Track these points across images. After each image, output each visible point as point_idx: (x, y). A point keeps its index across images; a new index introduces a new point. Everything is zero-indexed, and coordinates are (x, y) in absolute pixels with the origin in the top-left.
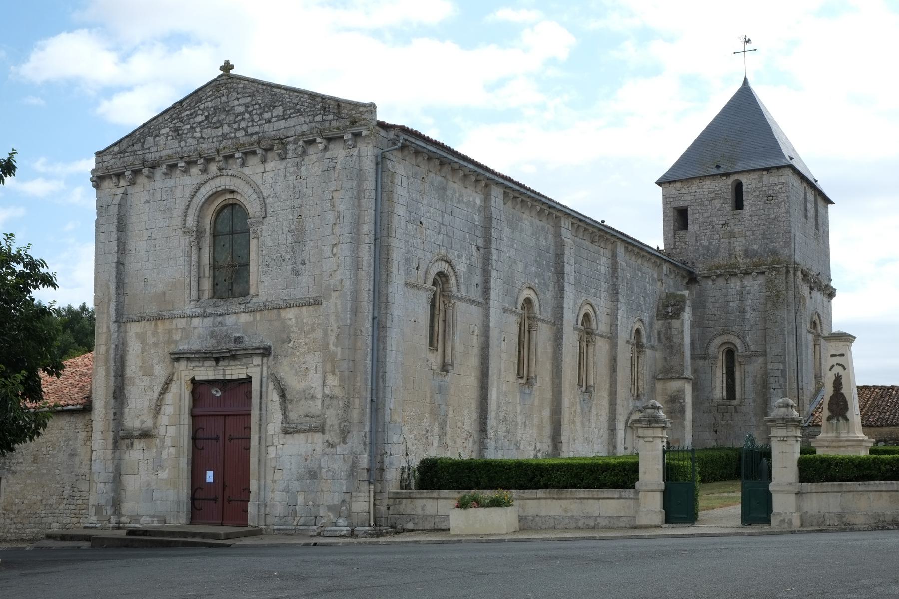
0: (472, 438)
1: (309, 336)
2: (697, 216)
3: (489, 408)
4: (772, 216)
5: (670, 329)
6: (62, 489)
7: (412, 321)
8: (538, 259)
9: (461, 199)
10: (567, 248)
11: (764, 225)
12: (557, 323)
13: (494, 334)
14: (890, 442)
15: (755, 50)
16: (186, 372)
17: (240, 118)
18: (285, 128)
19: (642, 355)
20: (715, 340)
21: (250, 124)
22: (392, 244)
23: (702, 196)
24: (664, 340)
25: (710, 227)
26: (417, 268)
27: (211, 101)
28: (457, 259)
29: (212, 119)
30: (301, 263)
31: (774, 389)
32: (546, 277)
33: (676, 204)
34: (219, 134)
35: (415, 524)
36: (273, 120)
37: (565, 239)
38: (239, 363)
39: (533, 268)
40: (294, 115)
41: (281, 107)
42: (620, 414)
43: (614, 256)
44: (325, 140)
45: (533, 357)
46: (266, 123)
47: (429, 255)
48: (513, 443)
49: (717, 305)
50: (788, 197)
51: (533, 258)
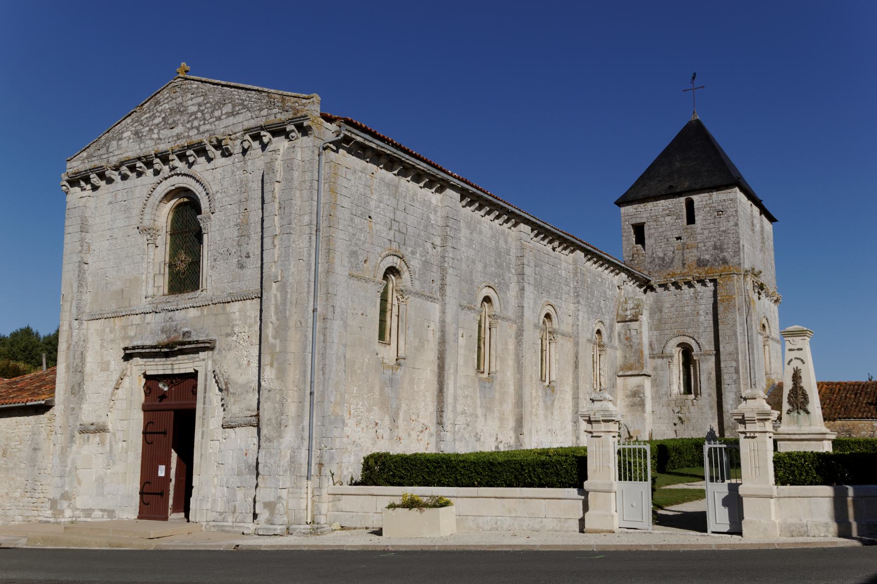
0: (428, 430)
1: (251, 329)
2: (652, 231)
3: (445, 401)
4: (722, 229)
5: (630, 330)
6: (25, 482)
7: (360, 314)
8: (498, 261)
9: (415, 197)
11: (715, 237)
12: (517, 321)
16: (139, 367)
17: (193, 117)
18: (233, 124)
19: (603, 353)
20: (672, 341)
21: (202, 123)
23: (657, 214)
25: (666, 240)
27: (167, 103)
28: (410, 255)
29: (168, 120)
30: (246, 257)
31: (729, 385)
32: (505, 278)
33: (634, 221)
34: (174, 134)
36: (224, 117)
39: (493, 269)
40: (242, 111)
41: (230, 104)
44: (268, 133)
45: (493, 352)
46: (216, 120)
47: (379, 250)
48: (473, 436)
49: (673, 309)
50: (736, 211)
51: (493, 259)
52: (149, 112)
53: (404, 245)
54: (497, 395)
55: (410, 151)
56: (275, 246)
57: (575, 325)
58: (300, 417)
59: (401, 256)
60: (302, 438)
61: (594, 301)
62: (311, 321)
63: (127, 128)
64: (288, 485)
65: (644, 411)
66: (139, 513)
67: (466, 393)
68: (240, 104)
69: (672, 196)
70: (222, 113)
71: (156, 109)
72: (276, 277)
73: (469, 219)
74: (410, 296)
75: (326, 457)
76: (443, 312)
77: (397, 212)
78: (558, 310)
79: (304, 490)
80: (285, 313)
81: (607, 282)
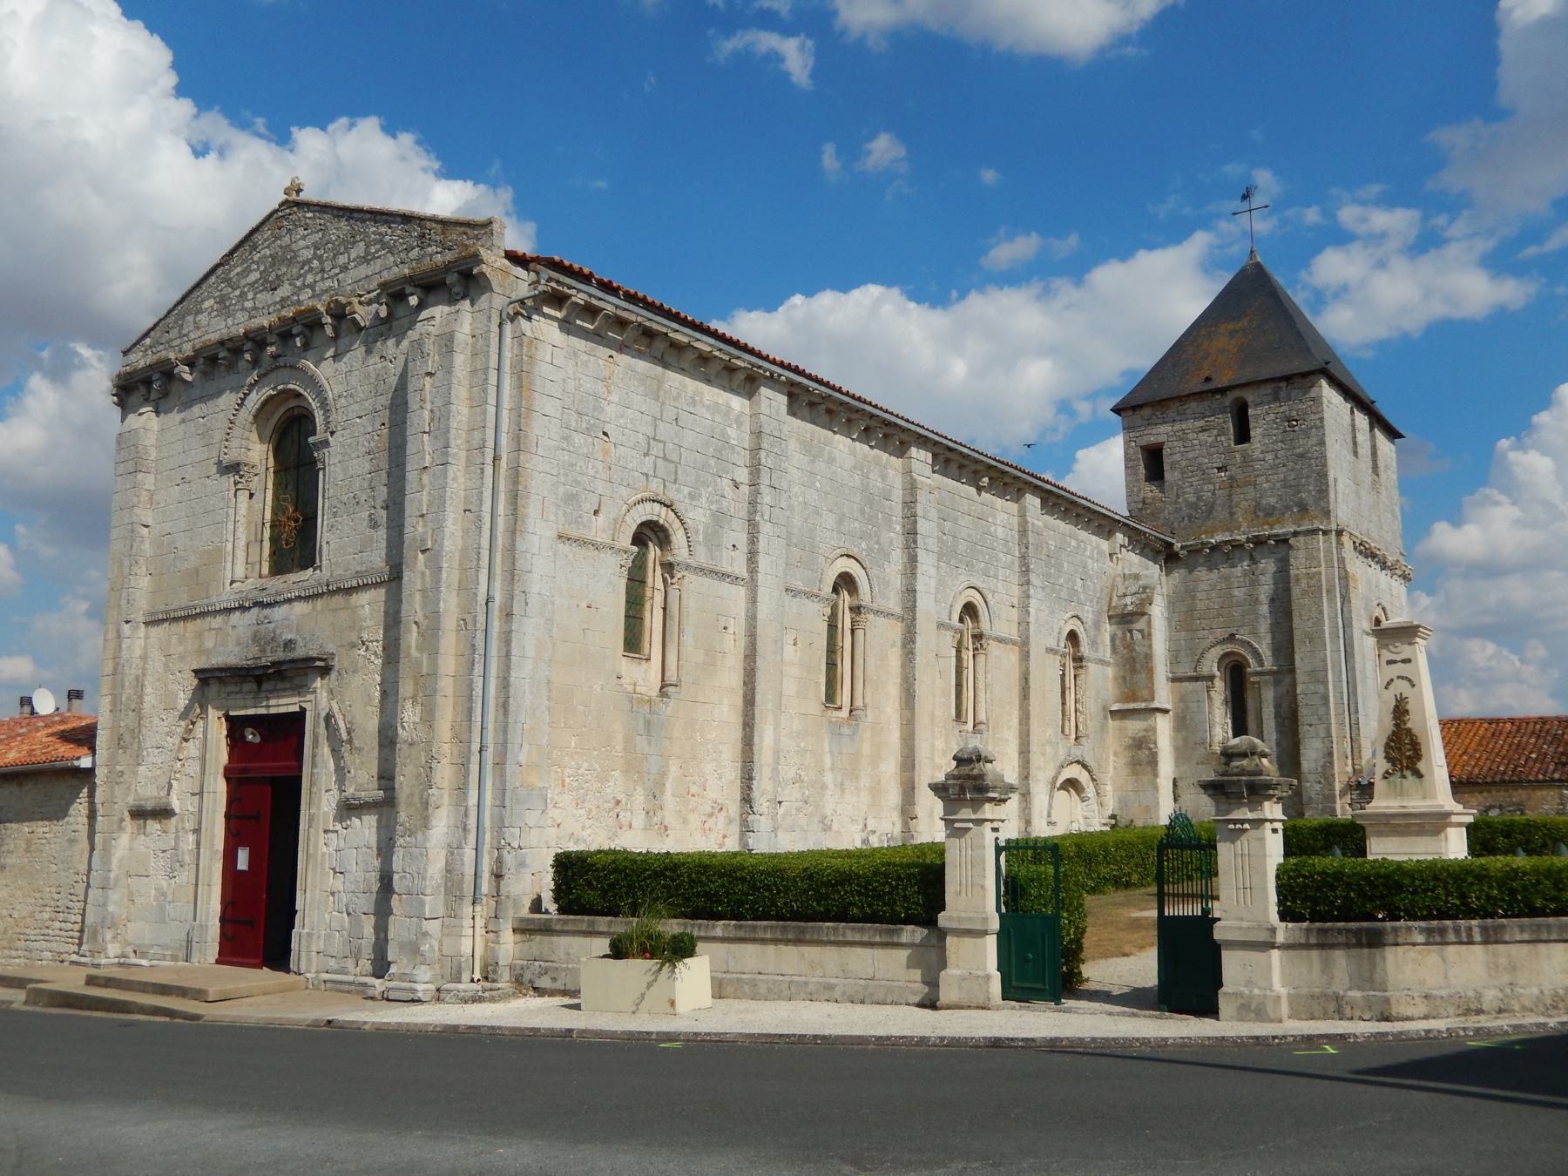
0: (724, 813)
7: (584, 605)
8: (867, 510)
9: (698, 399)
10: (922, 492)
13: (765, 633)
14: (1511, 809)
17: (306, 268)
19: (1081, 671)
21: (319, 277)
22: (527, 465)
24: (1120, 649)
26: (596, 512)
27: (268, 247)
35: (554, 979)
37: (918, 478)
38: (289, 686)
41: (363, 243)
42: (1039, 768)
43: (1022, 514)
44: (419, 290)
45: (859, 673)
46: (341, 272)
47: (624, 491)
48: (816, 821)
52: (242, 264)
53: (675, 482)
54: (866, 749)
55: (683, 315)
56: (423, 487)
57: (1024, 624)
58: (462, 790)
59: (667, 502)
60: (465, 829)
61: (1062, 581)
62: (481, 619)
63: (209, 292)
64: (441, 911)
65: (1156, 775)
66: (219, 953)
67: (802, 745)
68: (376, 242)
69: (1210, 394)
70: (349, 259)
71: (252, 259)
72: (423, 541)
73: (808, 435)
74: (686, 573)
75: (509, 859)
76: (753, 601)
77: (661, 425)
78: (989, 597)
79: (467, 922)
80: (438, 604)
81: (1089, 547)
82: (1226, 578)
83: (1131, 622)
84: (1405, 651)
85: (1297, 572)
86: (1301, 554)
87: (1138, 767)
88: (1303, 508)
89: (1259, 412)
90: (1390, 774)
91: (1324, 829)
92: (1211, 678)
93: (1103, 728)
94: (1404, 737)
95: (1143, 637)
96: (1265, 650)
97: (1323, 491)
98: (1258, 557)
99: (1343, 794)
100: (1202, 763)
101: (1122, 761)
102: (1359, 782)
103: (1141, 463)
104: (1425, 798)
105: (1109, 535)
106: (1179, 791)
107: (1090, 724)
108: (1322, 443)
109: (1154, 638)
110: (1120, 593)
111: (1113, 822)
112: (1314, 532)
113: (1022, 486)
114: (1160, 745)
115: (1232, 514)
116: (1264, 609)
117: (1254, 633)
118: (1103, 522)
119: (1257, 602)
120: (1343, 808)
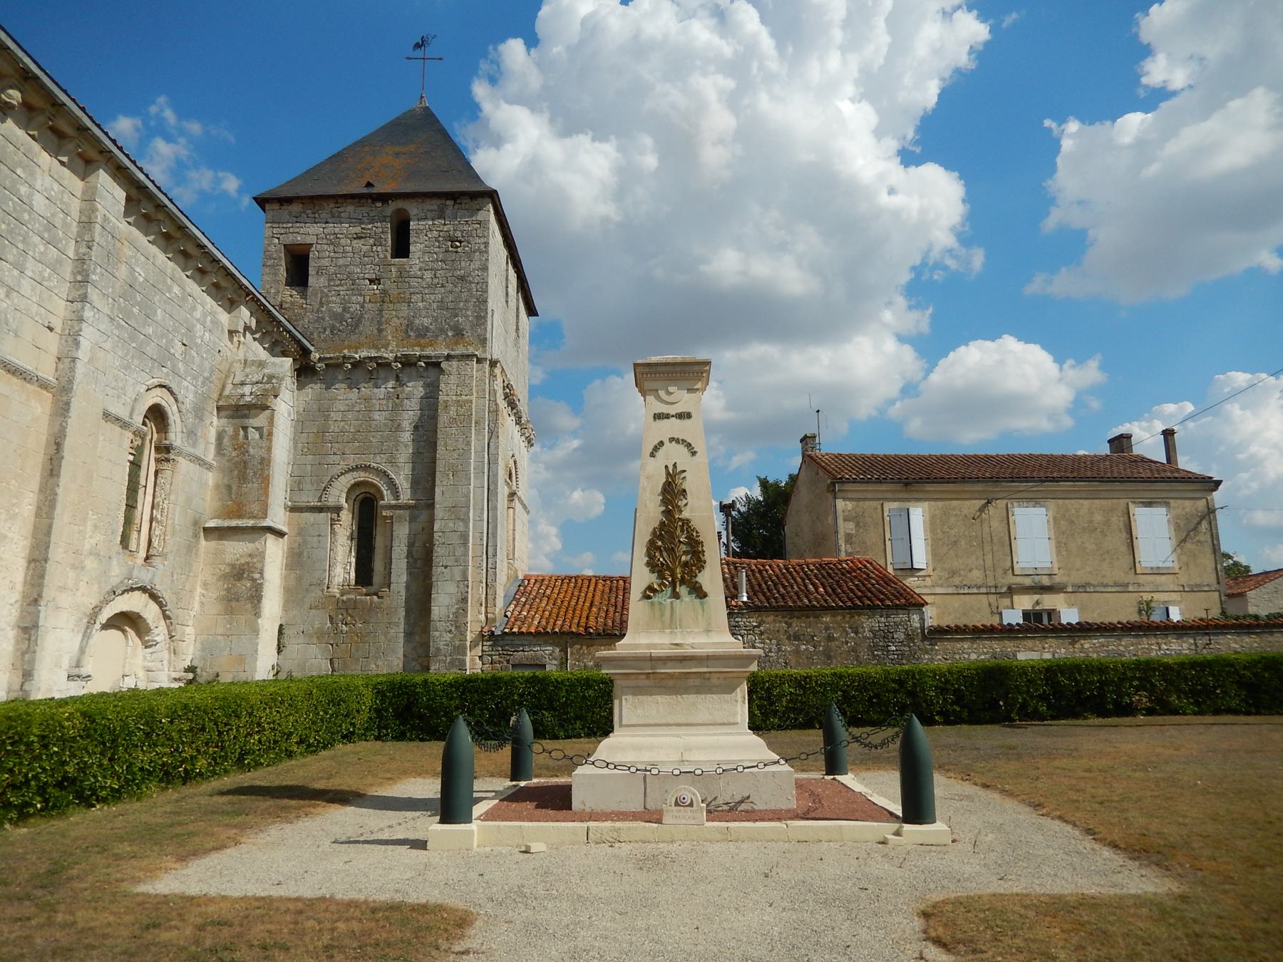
15: (441, 59)
19: (166, 466)
31: (446, 567)
42: (63, 588)
43: (89, 199)
57: (67, 359)
65: (257, 614)
69: (370, 201)
82: (367, 400)
83: (246, 417)
84: (682, 399)
85: (446, 398)
86: (453, 379)
87: (233, 604)
88: (459, 333)
89: (422, 227)
90: (655, 591)
91: (462, 684)
92: (338, 509)
93: (191, 549)
94: (678, 532)
95: (261, 437)
96: (403, 483)
97: (481, 317)
98: (405, 379)
99: (474, 644)
100: (316, 608)
101: (214, 594)
102: (493, 633)
103: (283, 263)
104: (708, 631)
105: (231, 305)
106: (285, 640)
107: (172, 536)
108: (485, 268)
109: (274, 439)
110: (237, 381)
111: (191, 676)
112: (469, 357)
113: (92, 154)
114: (267, 575)
115: (380, 331)
116: (407, 436)
117: (392, 462)
118: (224, 283)
119: (399, 428)
120: (472, 660)
